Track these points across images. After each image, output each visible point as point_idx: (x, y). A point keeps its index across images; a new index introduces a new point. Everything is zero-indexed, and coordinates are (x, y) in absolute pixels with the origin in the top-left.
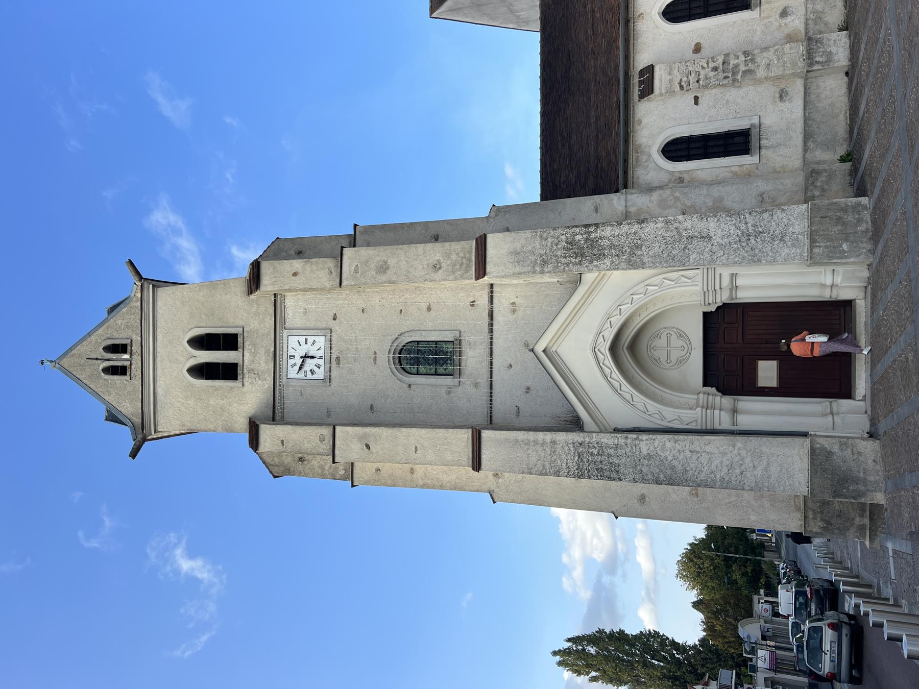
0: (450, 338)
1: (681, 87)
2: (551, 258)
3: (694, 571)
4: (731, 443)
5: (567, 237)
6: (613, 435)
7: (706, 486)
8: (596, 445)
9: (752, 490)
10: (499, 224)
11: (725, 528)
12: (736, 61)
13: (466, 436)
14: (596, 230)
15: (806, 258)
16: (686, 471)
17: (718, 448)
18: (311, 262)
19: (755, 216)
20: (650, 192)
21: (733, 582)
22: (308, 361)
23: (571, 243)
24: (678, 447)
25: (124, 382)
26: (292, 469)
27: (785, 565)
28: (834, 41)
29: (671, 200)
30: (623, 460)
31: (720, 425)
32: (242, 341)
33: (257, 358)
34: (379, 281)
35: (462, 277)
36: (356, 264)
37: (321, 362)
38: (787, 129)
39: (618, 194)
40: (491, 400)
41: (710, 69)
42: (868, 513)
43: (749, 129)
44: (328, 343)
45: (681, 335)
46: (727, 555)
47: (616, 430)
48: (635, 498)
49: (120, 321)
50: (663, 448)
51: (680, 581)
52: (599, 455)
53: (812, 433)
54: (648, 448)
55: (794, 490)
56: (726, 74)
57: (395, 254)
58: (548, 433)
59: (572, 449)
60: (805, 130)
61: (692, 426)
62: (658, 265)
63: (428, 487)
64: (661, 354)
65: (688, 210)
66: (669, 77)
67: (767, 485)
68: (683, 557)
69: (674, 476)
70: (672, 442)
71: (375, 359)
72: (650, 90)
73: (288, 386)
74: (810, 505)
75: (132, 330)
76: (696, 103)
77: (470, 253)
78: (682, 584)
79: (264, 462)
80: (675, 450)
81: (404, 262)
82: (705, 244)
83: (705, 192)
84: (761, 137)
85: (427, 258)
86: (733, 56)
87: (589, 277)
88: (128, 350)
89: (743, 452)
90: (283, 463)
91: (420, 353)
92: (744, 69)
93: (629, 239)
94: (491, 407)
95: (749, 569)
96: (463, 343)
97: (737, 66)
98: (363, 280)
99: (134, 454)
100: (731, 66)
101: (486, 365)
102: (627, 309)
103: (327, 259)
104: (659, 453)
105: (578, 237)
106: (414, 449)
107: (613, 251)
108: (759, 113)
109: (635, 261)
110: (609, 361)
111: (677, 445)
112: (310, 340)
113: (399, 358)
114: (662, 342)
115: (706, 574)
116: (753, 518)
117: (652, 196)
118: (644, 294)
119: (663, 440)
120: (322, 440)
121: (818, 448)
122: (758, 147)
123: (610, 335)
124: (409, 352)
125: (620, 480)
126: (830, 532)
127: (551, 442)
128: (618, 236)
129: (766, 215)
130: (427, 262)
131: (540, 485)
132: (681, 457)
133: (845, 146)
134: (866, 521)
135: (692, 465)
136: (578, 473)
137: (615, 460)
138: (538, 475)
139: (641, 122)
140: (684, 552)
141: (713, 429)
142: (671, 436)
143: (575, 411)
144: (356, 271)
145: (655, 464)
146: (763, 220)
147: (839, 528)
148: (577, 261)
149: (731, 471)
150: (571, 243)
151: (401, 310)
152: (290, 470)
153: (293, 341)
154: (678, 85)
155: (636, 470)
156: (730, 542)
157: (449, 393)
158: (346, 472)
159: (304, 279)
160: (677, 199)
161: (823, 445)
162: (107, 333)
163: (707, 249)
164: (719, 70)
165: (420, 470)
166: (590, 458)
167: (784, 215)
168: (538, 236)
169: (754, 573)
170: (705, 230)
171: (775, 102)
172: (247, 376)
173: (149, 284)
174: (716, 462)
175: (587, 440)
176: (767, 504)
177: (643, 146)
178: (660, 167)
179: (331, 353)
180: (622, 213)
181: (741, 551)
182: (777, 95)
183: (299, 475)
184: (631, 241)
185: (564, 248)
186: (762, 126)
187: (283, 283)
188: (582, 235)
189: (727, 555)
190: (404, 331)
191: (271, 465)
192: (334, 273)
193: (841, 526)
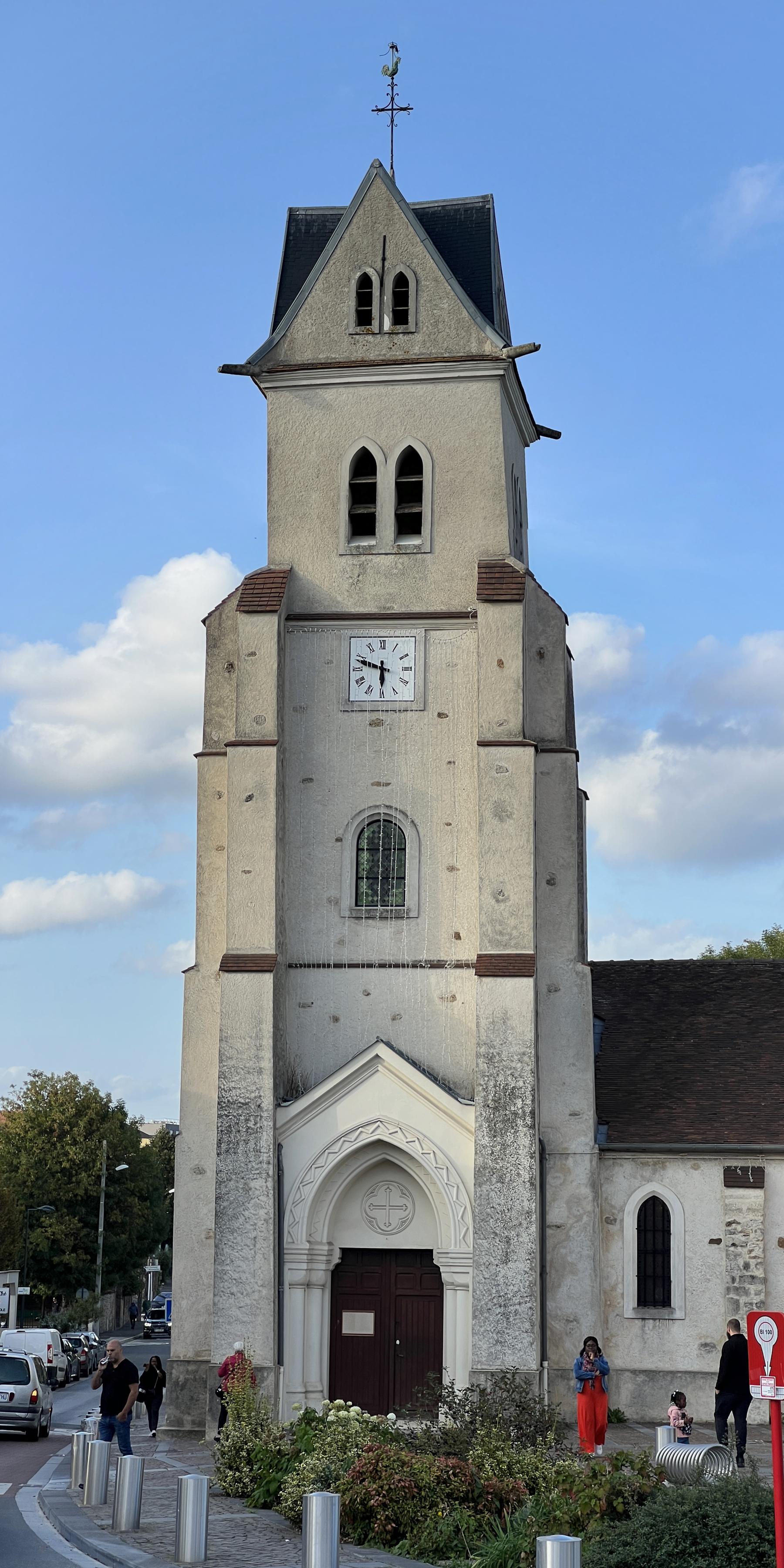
0: (410, 900)
1: (729, 1224)
2: (495, 1067)
3: (54, 1121)
4: (266, 1283)
5: (521, 1088)
6: (271, 1146)
7: (216, 1253)
8: (258, 1125)
9: (214, 1304)
10: (566, 978)
11: (171, 1192)
12: (753, 1292)
13: (266, 946)
14: (527, 1126)
15: (475, 1367)
16: (232, 1232)
17: (260, 1268)
18: (517, 692)
19: (527, 1314)
20: (591, 1185)
21: (33, 1222)
22: (378, 672)
23: (513, 1094)
24: (260, 1223)
25: (346, 322)
26: (216, 651)
27: (95, 1344)
28: (759, 1408)
29: (578, 1211)
30: (242, 1159)
31: (289, 1269)
32: (408, 552)
33: (383, 579)
34: (484, 807)
35: (484, 935)
36: (510, 769)
37: (376, 695)
38: (664, 1351)
39: (592, 1143)
40: (319, 966)
41: (748, 1260)
42: (196, 1429)
43: (670, 1305)
44: (403, 706)
45: (404, 1223)
46: (102, 1203)
47: (279, 1147)
48: (200, 1161)
49: (446, 306)
50: (258, 1206)
51: (26, 1083)
52: (247, 1129)
53: (282, 1370)
54: (258, 1188)
55: (217, 1349)
56: (738, 1280)
57: (521, 830)
58: (271, 1065)
59: (253, 1095)
60: (660, 1372)
61: (286, 1238)
62: (477, 1202)
63: (199, 874)
64: (381, 1197)
65: (564, 1232)
66: (745, 1208)
67: (221, 1320)
68: (86, 1089)
69: (226, 1218)
70: (266, 1217)
71: (378, 784)
72: (730, 1184)
73: (339, 638)
74: (203, 1367)
75: (430, 333)
76: (712, 1241)
77: (516, 946)
78: (17, 1089)
79: (224, 602)
80: (256, 1219)
81: (508, 846)
82: (499, 1258)
83: (586, 1252)
84: (658, 1321)
85: (513, 882)
86: (760, 1289)
87: (469, 1115)
88: (398, 327)
89: (256, 1296)
90: (224, 635)
91: (371, 881)
92: (741, 1301)
93: (511, 1168)
94: (309, 966)
95: (68, 1258)
96: (400, 922)
97: (747, 1293)
98: (485, 781)
99: (227, 369)
100: (747, 1286)
101: (359, 959)
102: (429, 1162)
103: (521, 718)
104: (252, 1201)
105: (519, 1103)
106: (247, 869)
107: (498, 1147)
108: (687, 1319)
109: (485, 1175)
110: (367, 1137)
111: (263, 1222)
112: (409, 676)
113: (379, 821)
114: (397, 1199)
115: (49, 1150)
116: (184, 1303)
117: (586, 1187)
118: (448, 1183)
119: (267, 1207)
120: (259, 720)
121: (263, 1374)
122: (644, 1317)
123: (397, 1140)
124: (387, 836)
125: (218, 1154)
126: (173, 1389)
127: (260, 1068)
128: (518, 1154)
129: (527, 1325)
130: (507, 880)
131: (209, 1036)
132: (248, 1226)
133: (635, 1417)
134: (188, 1427)
135: (239, 1238)
136: (225, 1103)
137: (241, 1148)
138: (220, 1051)
139: (696, 1169)
140: (102, 1094)
141: (284, 1254)
142: (272, 1216)
143: (317, 1085)
144: (500, 769)
145: (240, 1196)
146: (523, 1322)
147: (177, 1398)
148: (489, 1102)
149: (234, 1282)
150: (513, 1094)
151: (450, 824)
152: (214, 647)
153: (407, 646)
154: (732, 1219)
155: (231, 1173)
156: (135, 1210)
157: (329, 901)
158: (215, 742)
159: (493, 679)
160: (579, 1218)
161: (266, 1380)
162: (426, 279)
163: (492, 1259)
164: (745, 1271)
165: (220, 860)
166: (243, 1118)
167: (526, 1345)
168: (525, 1049)
169: (61, 1269)
170: (515, 1258)
171: (700, 1339)
172: (355, 563)
173: (505, 370)
174: (244, 1266)
175: (265, 1114)
176: (201, 1320)
177: (662, 1172)
178: (632, 1194)
179: (387, 711)
180: (566, 1148)
181: (114, 1239)
182: (708, 1341)
183: (207, 663)
184: (509, 1170)
185: (507, 1084)
186: (671, 1322)
187: (489, 644)
188: (521, 1108)
189: (102, 1203)
190: (420, 830)
191: (221, 615)
192: (500, 730)
193: (180, 1401)
